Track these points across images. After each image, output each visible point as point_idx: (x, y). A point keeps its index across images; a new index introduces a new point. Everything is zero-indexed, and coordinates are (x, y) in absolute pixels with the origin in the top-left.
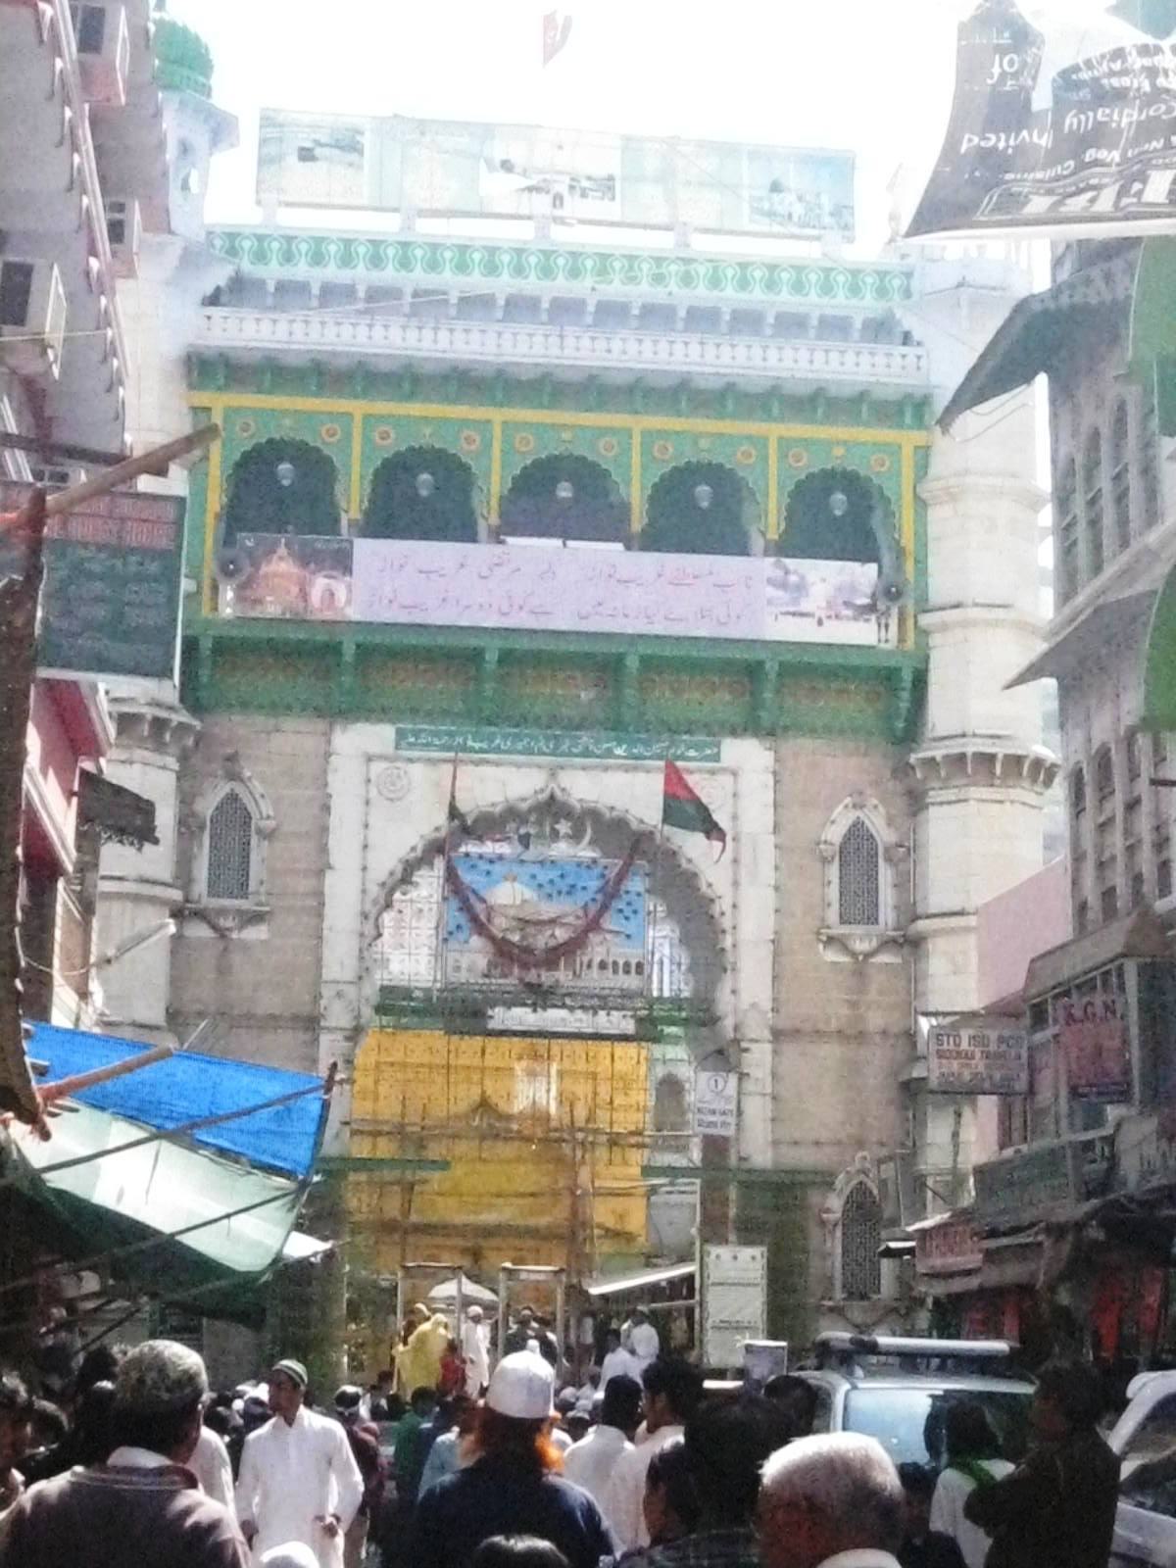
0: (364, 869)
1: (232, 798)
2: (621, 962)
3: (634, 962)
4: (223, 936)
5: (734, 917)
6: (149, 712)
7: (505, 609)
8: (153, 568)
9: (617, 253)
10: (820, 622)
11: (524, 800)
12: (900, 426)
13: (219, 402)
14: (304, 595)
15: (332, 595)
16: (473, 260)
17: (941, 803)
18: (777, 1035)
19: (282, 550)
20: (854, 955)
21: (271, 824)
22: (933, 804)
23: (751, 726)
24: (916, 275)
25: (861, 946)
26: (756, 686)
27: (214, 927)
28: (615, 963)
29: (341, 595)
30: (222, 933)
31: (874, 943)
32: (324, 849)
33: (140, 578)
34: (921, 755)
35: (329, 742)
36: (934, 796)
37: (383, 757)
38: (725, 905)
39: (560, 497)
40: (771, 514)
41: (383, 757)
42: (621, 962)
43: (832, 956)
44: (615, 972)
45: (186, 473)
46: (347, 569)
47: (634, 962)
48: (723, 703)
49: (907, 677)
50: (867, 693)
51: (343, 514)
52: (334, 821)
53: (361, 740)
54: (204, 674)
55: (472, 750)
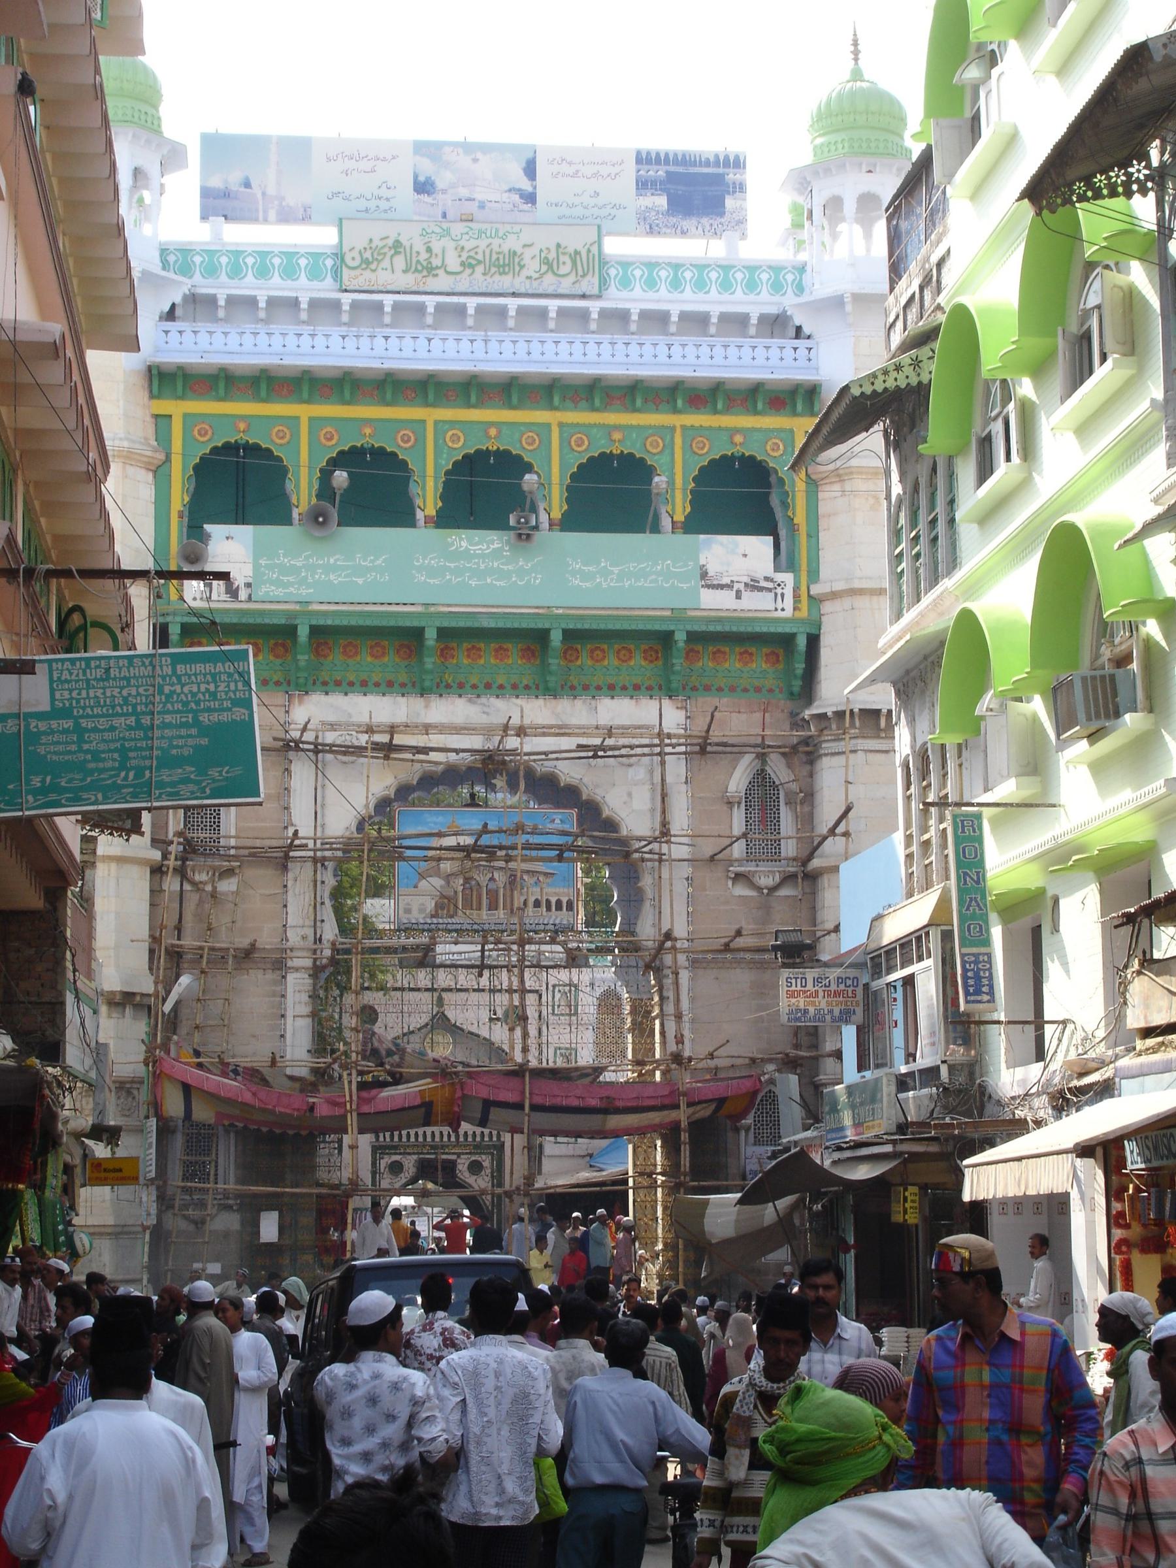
2: (553, 900)
3: (564, 900)
9: (172, 248)
12: (794, 414)
13: (177, 408)
16: (735, 279)
17: (833, 754)
20: (759, 889)
22: (826, 755)
24: (808, 268)
25: (765, 881)
26: (661, 651)
28: (548, 902)
31: (778, 879)
34: (815, 712)
36: (827, 747)
39: (485, 491)
40: (428, 496)
42: (553, 900)
43: (741, 891)
44: (549, 908)
45: (151, 475)
47: (564, 900)
49: (802, 642)
50: (645, 651)
51: (418, 511)
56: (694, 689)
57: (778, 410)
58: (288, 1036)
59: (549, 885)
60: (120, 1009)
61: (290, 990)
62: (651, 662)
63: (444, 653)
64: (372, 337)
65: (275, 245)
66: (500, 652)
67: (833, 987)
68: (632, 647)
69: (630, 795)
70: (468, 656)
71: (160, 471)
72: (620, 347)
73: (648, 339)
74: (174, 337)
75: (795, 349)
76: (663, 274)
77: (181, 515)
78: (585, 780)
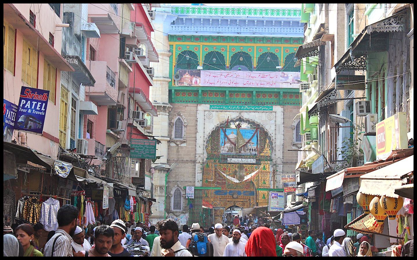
0: (204, 132)
1: (179, 119)
4: (178, 146)
5: (275, 140)
6: (163, 105)
7: (230, 83)
8: (153, 147)
10: (291, 84)
11: (235, 118)
13: (176, 43)
14: (191, 81)
15: (197, 81)
18: (284, 163)
19: (187, 73)
21: (186, 124)
23: (278, 104)
27: (176, 144)
29: (198, 81)
30: (177, 145)
32: (196, 129)
33: (152, 149)
35: (197, 108)
37: (207, 111)
38: (274, 138)
39: (242, 61)
41: (207, 111)
44: (253, 151)
46: (200, 76)
48: (273, 99)
52: (198, 123)
53: (202, 108)
54: (173, 97)
55: (224, 109)
56: (285, 103)
57: (287, 43)
58: (196, 177)
59: (253, 146)
60: (161, 171)
61: (196, 167)
62: (276, 97)
63: (231, 95)
64: (216, 27)
65: (298, 8)
66: (243, 96)
67: (291, 177)
68: (272, 94)
69: (271, 126)
70: (236, 96)
71: (170, 57)
72: (270, 29)
73: (276, 28)
74: (174, 28)
75: (275, 29)
76: (292, 12)
77: (175, 66)
78: (261, 123)
